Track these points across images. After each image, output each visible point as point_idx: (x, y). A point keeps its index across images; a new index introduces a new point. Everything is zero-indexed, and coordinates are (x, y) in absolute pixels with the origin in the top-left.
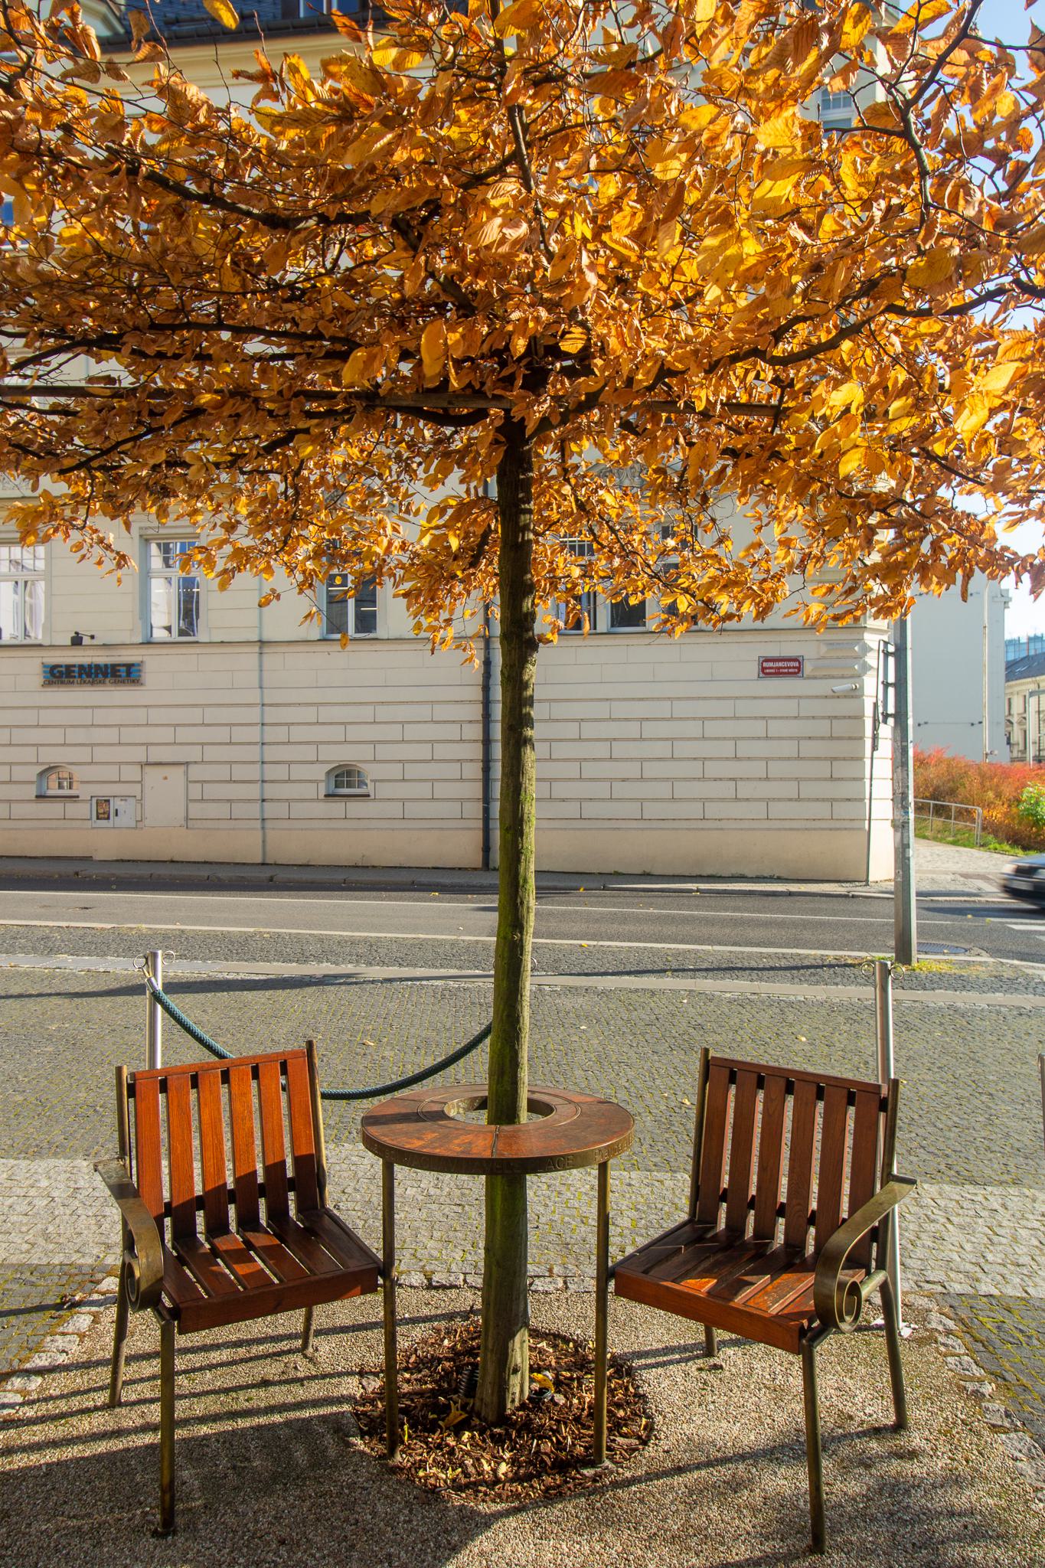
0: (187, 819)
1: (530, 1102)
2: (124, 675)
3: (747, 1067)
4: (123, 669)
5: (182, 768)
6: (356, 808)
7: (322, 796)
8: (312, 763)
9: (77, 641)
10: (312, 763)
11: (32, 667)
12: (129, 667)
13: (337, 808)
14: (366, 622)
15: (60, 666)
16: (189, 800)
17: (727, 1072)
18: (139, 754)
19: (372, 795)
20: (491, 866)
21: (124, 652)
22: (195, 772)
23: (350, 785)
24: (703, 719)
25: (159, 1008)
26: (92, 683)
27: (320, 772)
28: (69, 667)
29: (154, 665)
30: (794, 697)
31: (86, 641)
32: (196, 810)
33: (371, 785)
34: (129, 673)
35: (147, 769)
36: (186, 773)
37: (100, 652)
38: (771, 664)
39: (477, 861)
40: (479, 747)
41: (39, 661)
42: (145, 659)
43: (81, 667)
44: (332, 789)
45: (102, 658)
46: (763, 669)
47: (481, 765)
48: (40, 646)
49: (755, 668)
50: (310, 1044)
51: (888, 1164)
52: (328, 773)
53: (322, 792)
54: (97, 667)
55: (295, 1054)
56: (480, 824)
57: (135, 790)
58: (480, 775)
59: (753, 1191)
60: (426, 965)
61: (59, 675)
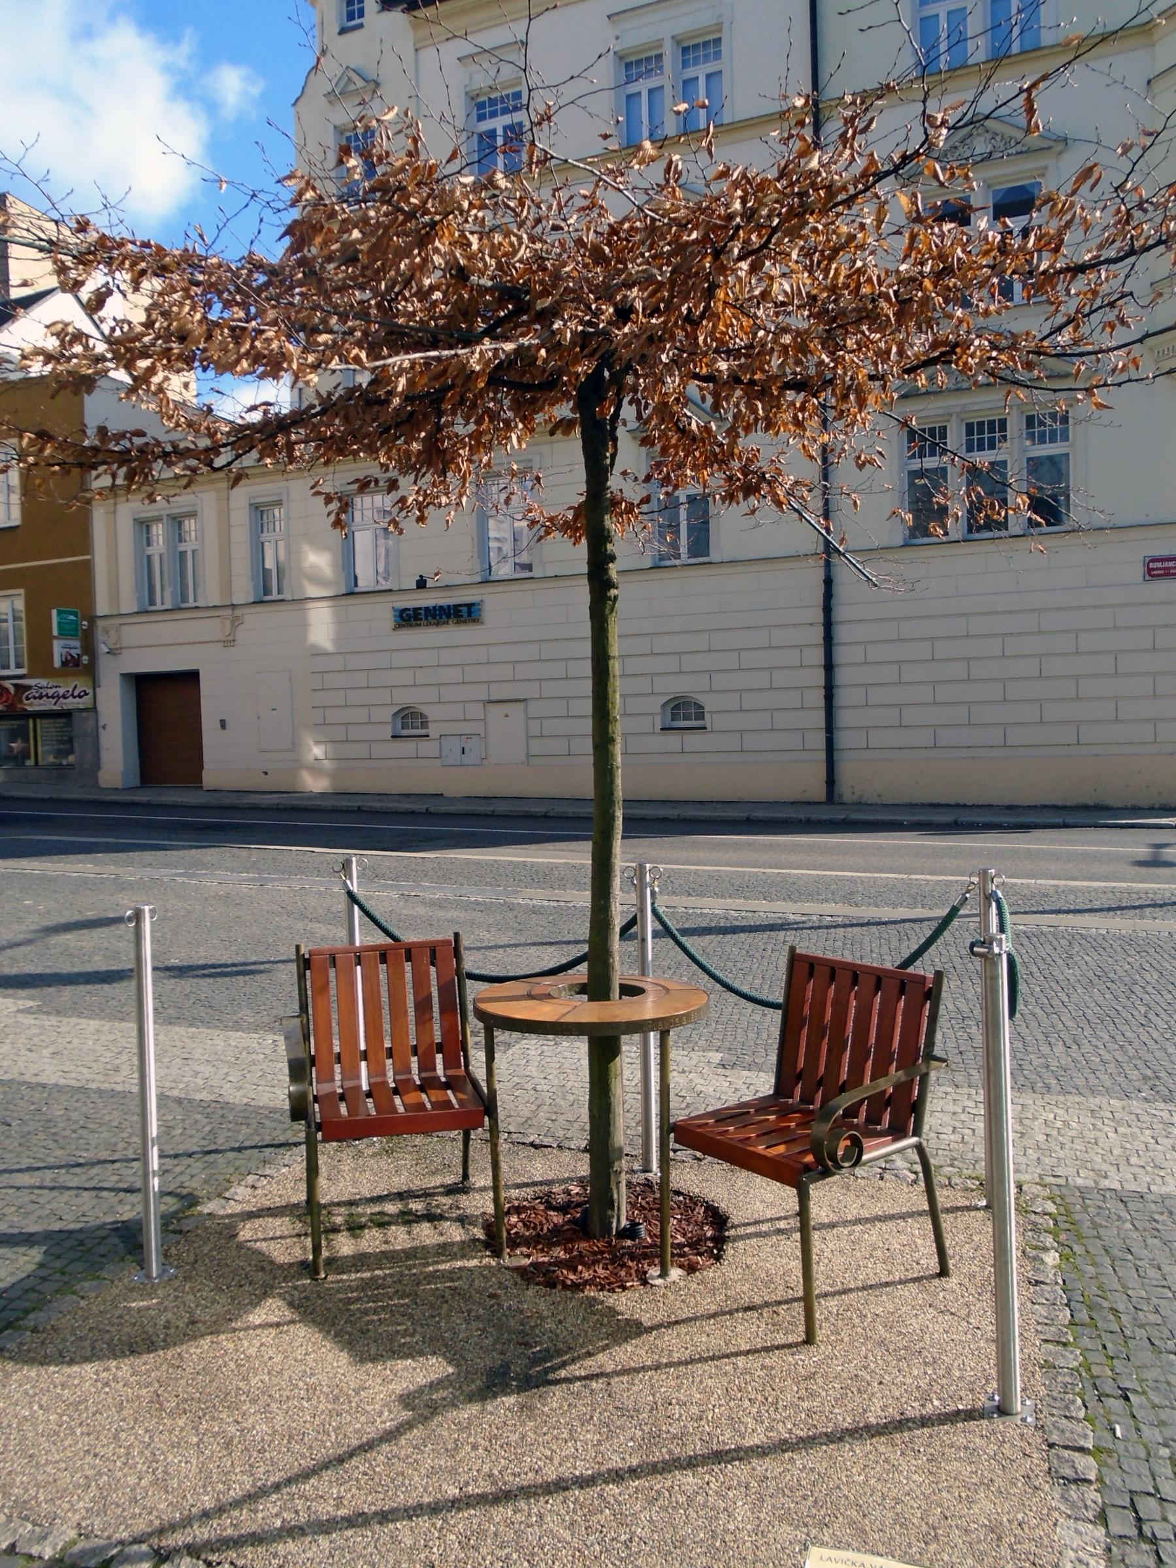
0: (528, 756)
1: (621, 986)
2: (465, 615)
3: (845, 966)
4: (465, 609)
5: (521, 706)
6: (693, 741)
7: (658, 730)
8: (648, 695)
9: (421, 584)
10: (648, 695)
11: (383, 612)
12: (470, 606)
13: (673, 741)
14: (700, 544)
15: (420, 609)
16: (529, 737)
17: (850, 974)
18: (482, 693)
19: (709, 729)
20: (836, 799)
21: (466, 592)
22: (535, 708)
23: (686, 717)
24: (1077, 631)
25: (356, 907)
26: (437, 624)
27: (656, 704)
28: (416, 610)
29: (493, 603)
30: (1033, 610)
31: (429, 584)
32: (537, 747)
33: (707, 716)
34: (470, 613)
35: (490, 707)
36: (526, 711)
37: (442, 594)
38: (1159, 565)
39: (822, 797)
40: (821, 673)
41: (391, 605)
42: (484, 598)
43: (427, 609)
44: (668, 724)
45: (444, 599)
46: (1150, 570)
47: (823, 692)
48: (391, 590)
49: (1140, 570)
50: (457, 935)
51: (930, 1043)
52: (395, 715)
53: (659, 726)
54: (441, 607)
55: (446, 943)
56: (822, 756)
57: (478, 728)
58: (822, 703)
59: (801, 1064)
60: (1096, 944)
61: (408, 618)
